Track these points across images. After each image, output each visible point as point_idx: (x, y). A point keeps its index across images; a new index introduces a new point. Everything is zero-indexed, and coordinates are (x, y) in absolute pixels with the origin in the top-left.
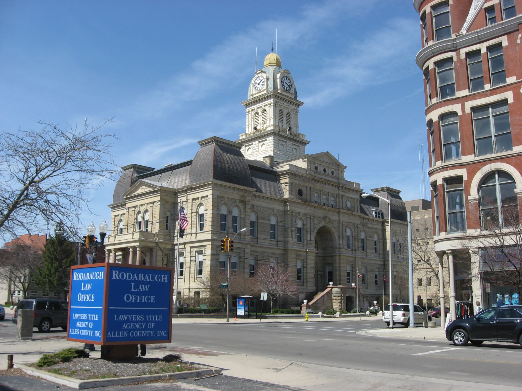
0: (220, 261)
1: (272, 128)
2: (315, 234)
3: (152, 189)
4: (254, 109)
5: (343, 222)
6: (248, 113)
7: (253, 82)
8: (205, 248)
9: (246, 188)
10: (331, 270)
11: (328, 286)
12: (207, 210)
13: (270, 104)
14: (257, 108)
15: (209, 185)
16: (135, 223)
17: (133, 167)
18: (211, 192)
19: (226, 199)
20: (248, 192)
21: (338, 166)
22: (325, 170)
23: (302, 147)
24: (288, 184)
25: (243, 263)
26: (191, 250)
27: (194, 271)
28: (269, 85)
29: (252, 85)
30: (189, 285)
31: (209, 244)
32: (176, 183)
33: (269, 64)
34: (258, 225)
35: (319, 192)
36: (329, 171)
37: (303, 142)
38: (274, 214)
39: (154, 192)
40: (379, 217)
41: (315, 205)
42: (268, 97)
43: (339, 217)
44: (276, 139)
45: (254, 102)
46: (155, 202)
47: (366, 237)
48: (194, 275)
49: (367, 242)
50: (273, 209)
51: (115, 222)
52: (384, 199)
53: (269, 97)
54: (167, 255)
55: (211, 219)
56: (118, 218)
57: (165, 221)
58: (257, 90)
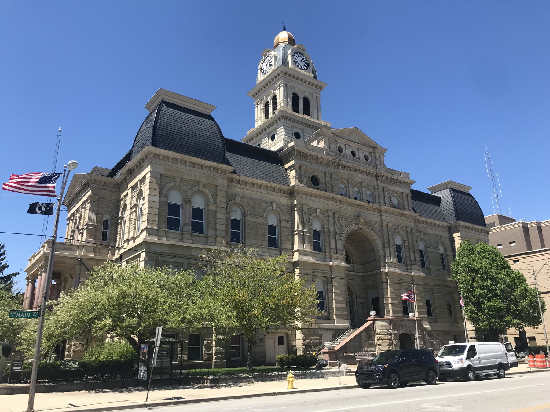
9: (215, 164)
10: (375, 296)
11: (369, 318)
13: (280, 85)
19: (178, 180)
22: (353, 153)
52: (445, 195)
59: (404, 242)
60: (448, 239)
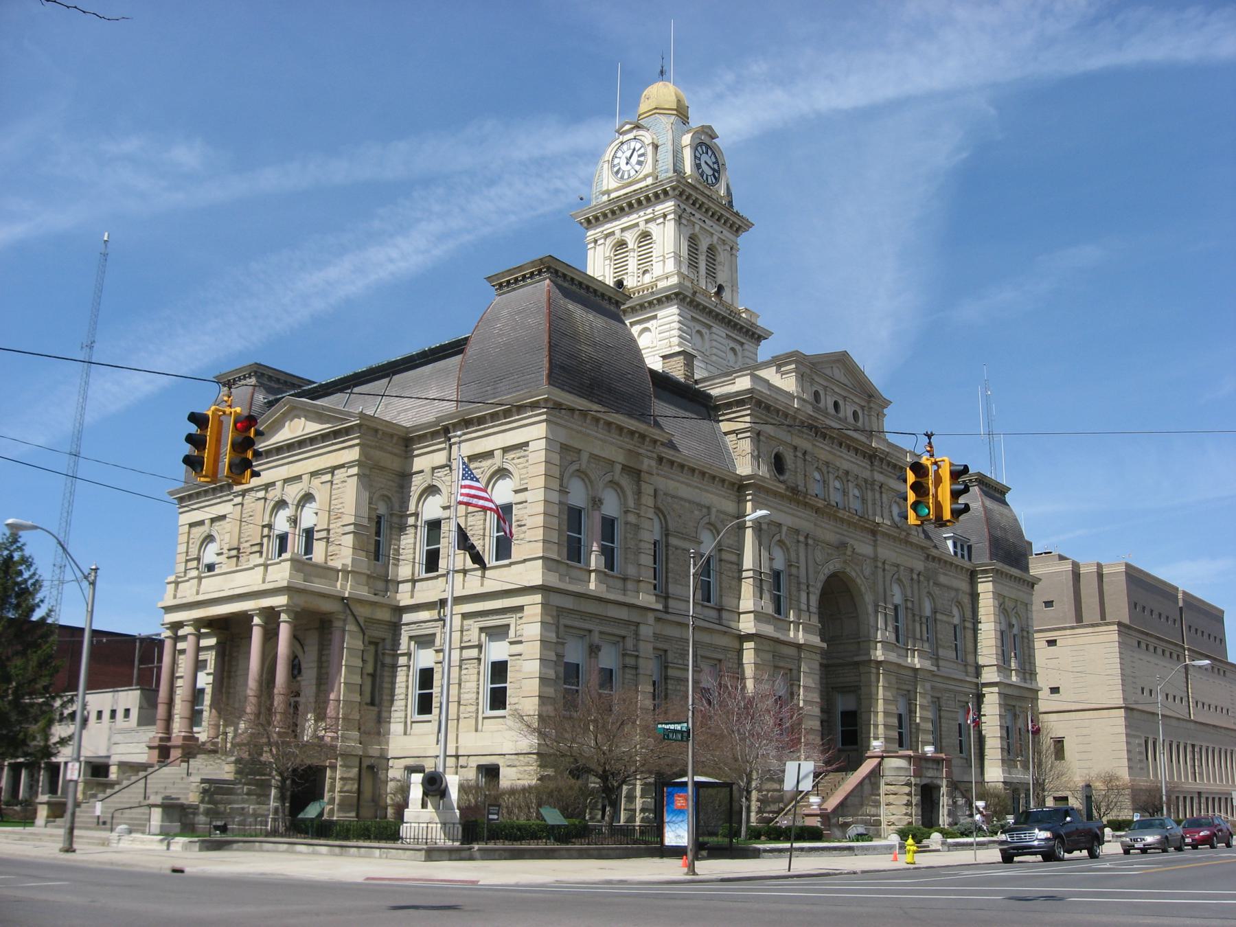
0: (566, 663)
1: (674, 280)
2: (818, 592)
3: (330, 425)
4: (613, 233)
5: (884, 563)
6: (593, 245)
7: (608, 155)
8: (519, 615)
12: (526, 489)
13: (665, 216)
14: (623, 230)
15: (534, 406)
16: (265, 540)
17: (256, 372)
18: (540, 430)
19: (585, 457)
20: (646, 443)
21: (870, 396)
23: (749, 345)
24: (748, 434)
25: (633, 672)
26: (462, 626)
27: (474, 696)
28: (660, 164)
29: (606, 166)
30: (457, 742)
31: (533, 605)
32: (406, 410)
33: (656, 108)
34: (667, 554)
35: (824, 469)
36: (847, 410)
37: (754, 333)
38: (709, 523)
39: (336, 434)
40: (963, 556)
41: (819, 505)
42: (659, 196)
43: (875, 546)
44: (685, 315)
45: (613, 212)
46: (342, 466)
47: (935, 612)
48: (473, 708)
49: (939, 626)
50: (709, 508)
51: (188, 543)
53: (662, 196)
54: (376, 644)
55: (540, 520)
56: (199, 532)
57: (373, 531)
58: (622, 177)
59: (906, 600)
60: (967, 596)
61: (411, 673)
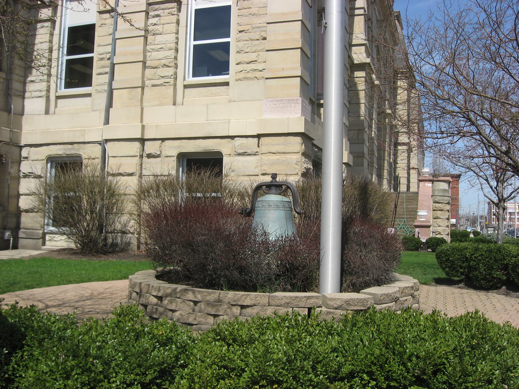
30: (142, 121)
61: (56, 32)
